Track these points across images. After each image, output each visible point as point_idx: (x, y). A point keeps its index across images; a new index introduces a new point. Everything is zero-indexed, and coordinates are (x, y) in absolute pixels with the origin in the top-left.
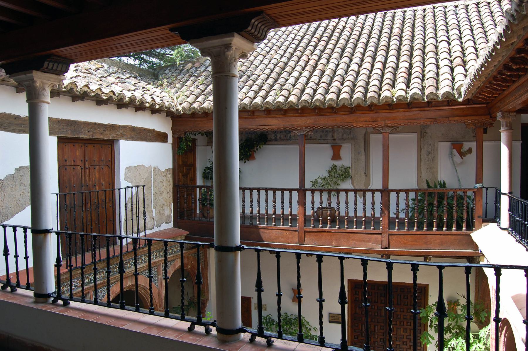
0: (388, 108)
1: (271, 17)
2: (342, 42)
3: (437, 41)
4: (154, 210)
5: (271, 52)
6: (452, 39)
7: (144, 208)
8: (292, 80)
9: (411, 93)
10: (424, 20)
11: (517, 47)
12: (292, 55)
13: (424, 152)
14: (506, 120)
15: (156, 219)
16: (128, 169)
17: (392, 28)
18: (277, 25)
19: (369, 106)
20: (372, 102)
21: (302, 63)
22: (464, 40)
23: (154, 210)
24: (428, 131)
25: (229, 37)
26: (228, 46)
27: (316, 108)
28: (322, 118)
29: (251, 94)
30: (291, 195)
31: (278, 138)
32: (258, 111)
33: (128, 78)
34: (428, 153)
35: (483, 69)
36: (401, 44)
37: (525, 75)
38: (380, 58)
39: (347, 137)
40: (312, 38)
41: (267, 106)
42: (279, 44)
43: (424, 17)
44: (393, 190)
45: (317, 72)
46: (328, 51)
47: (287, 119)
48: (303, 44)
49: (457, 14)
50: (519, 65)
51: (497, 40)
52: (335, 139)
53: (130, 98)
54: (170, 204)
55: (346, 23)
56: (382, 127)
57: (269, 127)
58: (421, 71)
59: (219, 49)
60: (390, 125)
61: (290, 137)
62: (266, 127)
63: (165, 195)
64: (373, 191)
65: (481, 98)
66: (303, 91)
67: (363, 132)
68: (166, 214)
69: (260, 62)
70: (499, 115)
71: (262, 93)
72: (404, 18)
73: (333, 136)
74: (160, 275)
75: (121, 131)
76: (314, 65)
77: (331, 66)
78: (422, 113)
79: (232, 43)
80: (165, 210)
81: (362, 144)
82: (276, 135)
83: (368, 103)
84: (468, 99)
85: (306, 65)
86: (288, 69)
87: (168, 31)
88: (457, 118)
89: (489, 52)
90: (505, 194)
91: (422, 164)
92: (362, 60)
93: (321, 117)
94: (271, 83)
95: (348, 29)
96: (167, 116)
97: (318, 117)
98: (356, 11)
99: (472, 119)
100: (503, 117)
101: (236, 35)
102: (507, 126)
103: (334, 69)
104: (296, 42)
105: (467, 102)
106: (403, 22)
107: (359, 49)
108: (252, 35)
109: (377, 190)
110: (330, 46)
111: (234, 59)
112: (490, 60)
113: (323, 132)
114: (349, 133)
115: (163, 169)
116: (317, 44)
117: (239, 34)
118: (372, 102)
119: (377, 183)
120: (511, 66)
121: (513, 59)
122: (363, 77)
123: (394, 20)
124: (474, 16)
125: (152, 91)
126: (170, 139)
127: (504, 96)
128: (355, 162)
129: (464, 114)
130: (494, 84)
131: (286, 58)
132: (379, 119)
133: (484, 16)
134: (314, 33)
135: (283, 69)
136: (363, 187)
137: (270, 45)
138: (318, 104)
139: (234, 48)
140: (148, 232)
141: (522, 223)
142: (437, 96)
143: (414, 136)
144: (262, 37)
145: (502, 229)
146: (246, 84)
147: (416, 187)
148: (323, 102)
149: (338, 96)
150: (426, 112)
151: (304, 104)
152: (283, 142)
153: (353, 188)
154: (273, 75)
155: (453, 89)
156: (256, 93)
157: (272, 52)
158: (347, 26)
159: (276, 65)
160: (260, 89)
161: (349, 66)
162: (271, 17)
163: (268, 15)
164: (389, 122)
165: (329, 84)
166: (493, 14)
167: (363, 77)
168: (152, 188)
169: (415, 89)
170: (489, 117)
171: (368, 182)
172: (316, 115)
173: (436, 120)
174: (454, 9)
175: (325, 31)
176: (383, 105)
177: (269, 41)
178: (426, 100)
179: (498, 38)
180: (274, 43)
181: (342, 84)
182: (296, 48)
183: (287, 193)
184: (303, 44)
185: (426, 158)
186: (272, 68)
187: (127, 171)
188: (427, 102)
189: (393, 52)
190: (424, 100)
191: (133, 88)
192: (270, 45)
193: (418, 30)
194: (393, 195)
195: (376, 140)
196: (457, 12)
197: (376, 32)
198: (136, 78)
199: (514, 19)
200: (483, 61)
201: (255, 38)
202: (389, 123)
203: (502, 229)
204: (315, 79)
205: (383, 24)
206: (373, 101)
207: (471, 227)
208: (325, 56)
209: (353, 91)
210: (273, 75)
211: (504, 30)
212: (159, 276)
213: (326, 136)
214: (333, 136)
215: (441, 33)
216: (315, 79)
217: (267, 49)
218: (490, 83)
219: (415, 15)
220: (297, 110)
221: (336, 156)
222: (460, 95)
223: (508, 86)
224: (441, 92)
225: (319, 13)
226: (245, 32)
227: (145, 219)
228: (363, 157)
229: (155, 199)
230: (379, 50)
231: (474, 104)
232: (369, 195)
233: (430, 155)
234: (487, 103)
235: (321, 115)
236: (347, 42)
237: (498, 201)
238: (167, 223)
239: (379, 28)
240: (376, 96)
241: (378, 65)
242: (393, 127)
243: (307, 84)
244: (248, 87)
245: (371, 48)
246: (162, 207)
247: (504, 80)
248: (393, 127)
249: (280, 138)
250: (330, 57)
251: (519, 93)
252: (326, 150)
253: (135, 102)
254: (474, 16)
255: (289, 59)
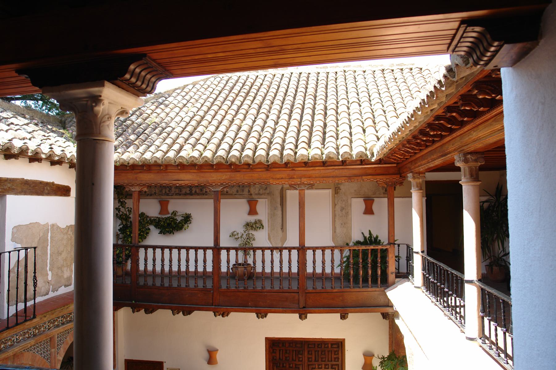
0: (304, 165)
1: (159, 64)
2: (259, 98)
3: (348, 102)
4: (50, 273)
5: (188, 105)
6: (362, 100)
7: (35, 273)
8: (208, 135)
9: (326, 152)
10: (336, 82)
11: (436, 114)
12: (209, 109)
13: (338, 208)
14: (417, 180)
15: (53, 283)
16: (17, 229)
17: (307, 88)
18: (169, 74)
19: (285, 163)
20: (288, 160)
21: (219, 117)
22: (372, 102)
23: (50, 273)
24: (342, 187)
25: (97, 87)
26: (97, 99)
27: (232, 164)
28: (238, 174)
29: (164, 148)
30: (205, 254)
31: (193, 192)
32: (171, 165)
33: (27, 124)
34: (342, 209)
35: (400, 133)
36: (315, 104)
37: (440, 140)
38: (296, 115)
39: (264, 192)
40: (229, 93)
41: (181, 161)
42: (196, 97)
43: (336, 79)
44: (309, 248)
45: (234, 128)
46: (245, 107)
47: (202, 175)
48: (221, 99)
49: (365, 78)
50: (437, 131)
51: (419, 106)
52: (251, 194)
53: (20, 148)
54: (71, 264)
55: (263, 81)
56: (298, 185)
57: (182, 182)
58: (335, 130)
59: (85, 102)
60: (306, 183)
61: (206, 192)
62: (180, 182)
63: (64, 255)
64: (290, 249)
65: (393, 159)
66: (218, 146)
67: (280, 187)
68: (65, 276)
69: (176, 114)
70: (410, 175)
71: (176, 147)
72: (318, 80)
73: (249, 191)
74: (54, 348)
75: (9, 185)
76: (231, 119)
77: (249, 121)
78: (336, 171)
79: (103, 95)
80: (65, 272)
81: (279, 200)
82: (191, 189)
83: (285, 160)
84: (380, 159)
85: (223, 119)
86: (204, 123)
87: (14, 74)
88: (370, 177)
89: (408, 117)
90: (417, 253)
91: (336, 220)
92: (279, 117)
93: (238, 173)
94: (186, 137)
95: (266, 87)
96: (70, 167)
97: (233, 173)
98: (271, 62)
99: (384, 178)
100: (414, 178)
101: (107, 83)
102: (417, 187)
103: (251, 124)
104: (214, 96)
105: (379, 161)
106: (317, 83)
107: (276, 107)
108: (133, 85)
109: (294, 248)
110: (248, 102)
111: (107, 117)
112: (408, 125)
113: (239, 186)
114: (266, 190)
115: (63, 225)
116: (234, 100)
117: (113, 84)
118: (288, 160)
119: (293, 240)
120: (428, 131)
121: (430, 125)
122: (279, 134)
123: (308, 80)
124: (380, 81)
125: (52, 141)
126: (73, 192)
127: (415, 158)
128: (271, 218)
129: (375, 173)
130: (408, 148)
131: (203, 112)
132: (295, 177)
133: (390, 81)
134: (232, 88)
135: (199, 123)
136: (279, 245)
137: (187, 97)
138: (233, 160)
139: (106, 102)
140: (39, 299)
141: (438, 286)
142: (351, 155)
143: (328, 193)
144: (149, 89)
145: (415, 287)
146: (160, 137)
147: (332, 244)
148: (239, 159)
149: (255, 152)
150: (341, 170)
151: (219, 160)
152: (198, 197)
153: (271, 246)
154: (190, 128)
155: (366, 150)
156: (170, 146)
157: (189, 105)
158: (264, 83)
159: (192, 118)
160: (174, 142)
161: (265, 122)
162: (159, 64)
163: (154, 60)
164: (305, 179)
165: (246, 141)
166: (397, 80)
167: (279, 134)
168: (49, 248)
169: (330, 149)
170: (399, 176)
171: (284, 239)
172: (232, 172)
173: (350, 178)
174: (363, 73)
175: (242, 87)
176: (300, 163)
177: (187, 93)
178: (341, 159)
179: (420, 103)
180: (192, 96)
181: (259, 141)
182: (214, 102)
183: (201, 252)
184: (221, 99)
185: (340, 214)
186: (188, 121)
187: (15, 230)
188: (342, 161)
189: (308, 111)
190: (338, 159)
191: (29, 136)
192: (187, 97)
193: (331, 91)
194: (309, 253)
195: (292, 195)
196: (365, 76)
197: (291, 91)
198: (36, 125)
199: (442, 86)
200: (400, 126)
201: (138, 90)
202: (305, 181)
203: (415, 287)
204: (231, 134)
205: (298, 83)
206: (289, 158)
207: (386, 283)
208: (242, 111)
209: (269, 148)
210: (190, 128)
211: (427, 96)
212: (53, 350)
213: (243, 191)
214: (249, 191)
215: (352, 96)
216: (231, 134)
217: (185, 102)
218: (404, 146)
219: (328, 77)
220: (212, 166)
221: (252, 211)
222: (373, 155)
223: (421, 150)
224: (354, 153)
225: (223, 63)
226: (122, 81)
227: (35, 285)
228: (279, 212)
229: (52, 260)
230: (294, 108)
231: (385, 164)
232: (285, 253)
233: (344, 211)
234: (397, 164)
235: (237, 171)
236: (264, 99)
237: (409, 258)
238: (66, 286)
239: (295, 87)
240: (292, 153)
241: (294, 123)
242: (309, 184)
243: (223, 139)
244: (161, 140)
245: (287, 105)
246: (60, 268)
247: (418, 144)
248: (309, 184)
249: (196, 192)
250: (247, 112)
251: (432, 157)
252: (242, 205)
253: (28, 153)
254: (380, 81)
255: (206, 113)
